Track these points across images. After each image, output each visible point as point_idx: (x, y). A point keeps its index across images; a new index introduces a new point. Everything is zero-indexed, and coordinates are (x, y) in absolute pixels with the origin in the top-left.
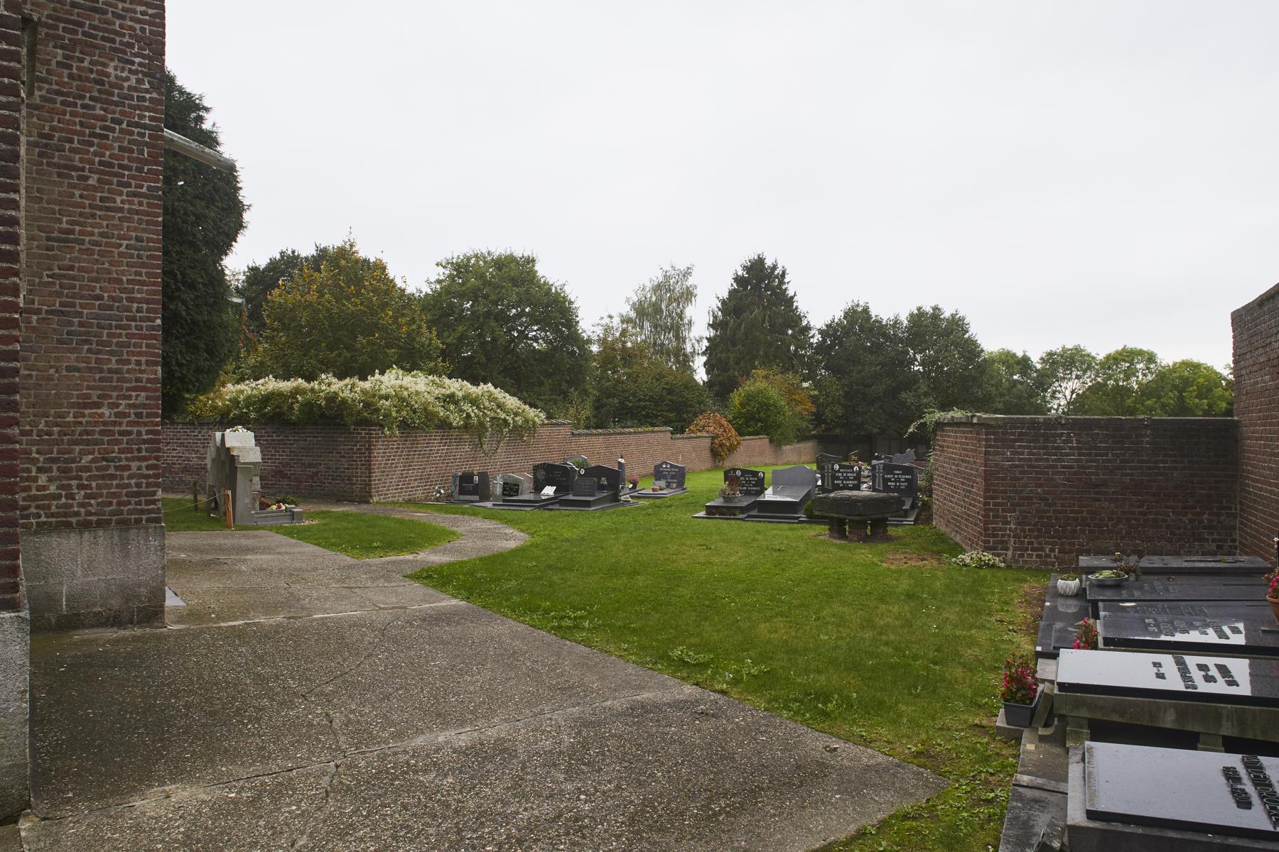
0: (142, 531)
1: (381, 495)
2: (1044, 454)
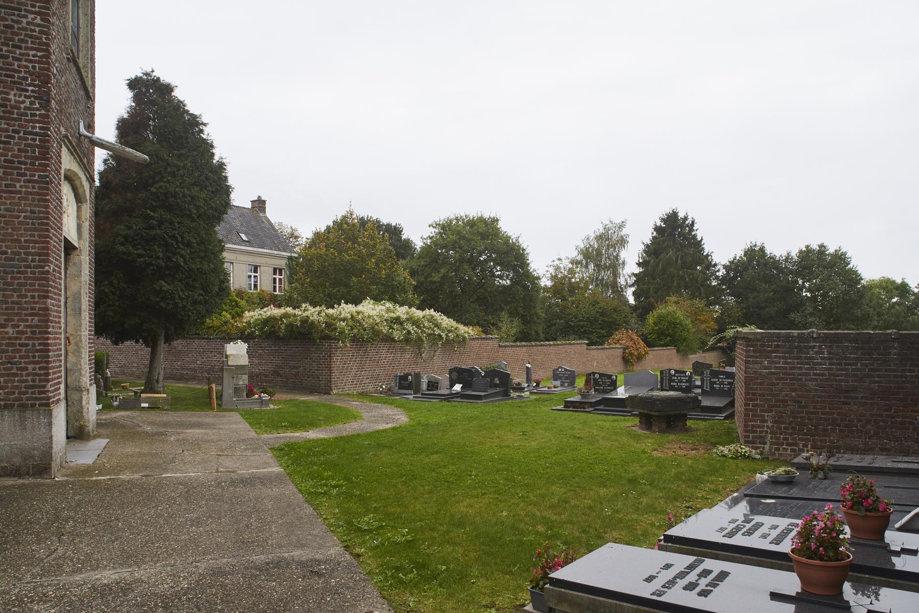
0: (35, 412)
1: (340, 389)
2: (798, 363)
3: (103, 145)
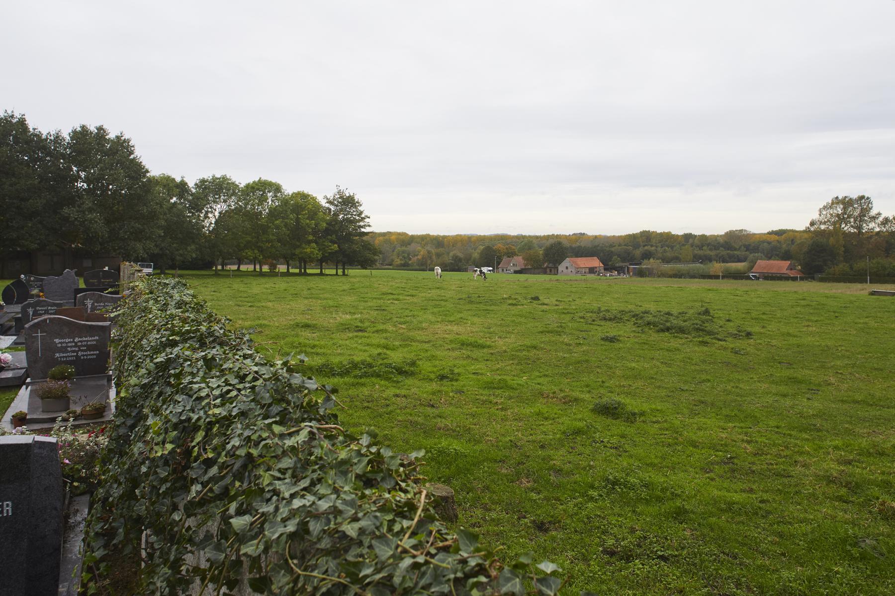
3: (143, 549)
